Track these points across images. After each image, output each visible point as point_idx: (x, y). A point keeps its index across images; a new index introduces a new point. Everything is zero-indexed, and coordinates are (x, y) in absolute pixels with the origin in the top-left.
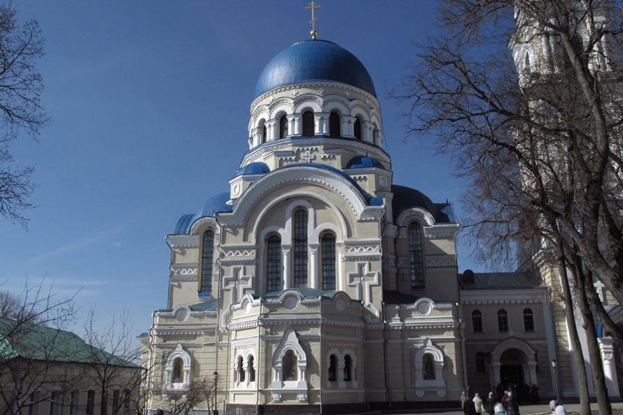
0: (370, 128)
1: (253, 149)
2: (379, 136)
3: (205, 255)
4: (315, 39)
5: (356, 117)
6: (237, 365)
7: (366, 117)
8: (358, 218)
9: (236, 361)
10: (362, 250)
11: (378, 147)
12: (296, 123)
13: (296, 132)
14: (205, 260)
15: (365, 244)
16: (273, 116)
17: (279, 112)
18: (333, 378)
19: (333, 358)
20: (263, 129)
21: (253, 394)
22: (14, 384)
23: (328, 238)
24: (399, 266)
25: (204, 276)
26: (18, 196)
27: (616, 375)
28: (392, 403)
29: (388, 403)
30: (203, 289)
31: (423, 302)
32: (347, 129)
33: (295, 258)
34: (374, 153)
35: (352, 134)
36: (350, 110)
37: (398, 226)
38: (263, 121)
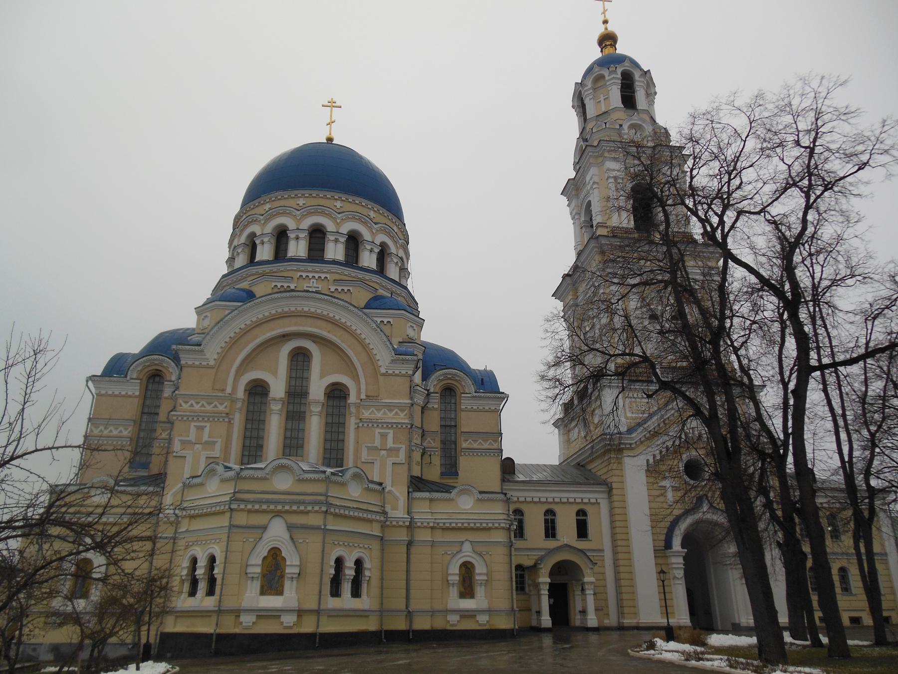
3: (146, 410)
9: (186, 563)
10: (397, 414)
14: (145, 417)
15: (390, 407)
21: (210, 616)
22: (626, 429)
23: (337, 393)
25: (141, 441)
27: (716, 602)
28: (413, 631)
29: (408, 631)
32: (368, 259)
33: (287, 420)
38: (253, 235)
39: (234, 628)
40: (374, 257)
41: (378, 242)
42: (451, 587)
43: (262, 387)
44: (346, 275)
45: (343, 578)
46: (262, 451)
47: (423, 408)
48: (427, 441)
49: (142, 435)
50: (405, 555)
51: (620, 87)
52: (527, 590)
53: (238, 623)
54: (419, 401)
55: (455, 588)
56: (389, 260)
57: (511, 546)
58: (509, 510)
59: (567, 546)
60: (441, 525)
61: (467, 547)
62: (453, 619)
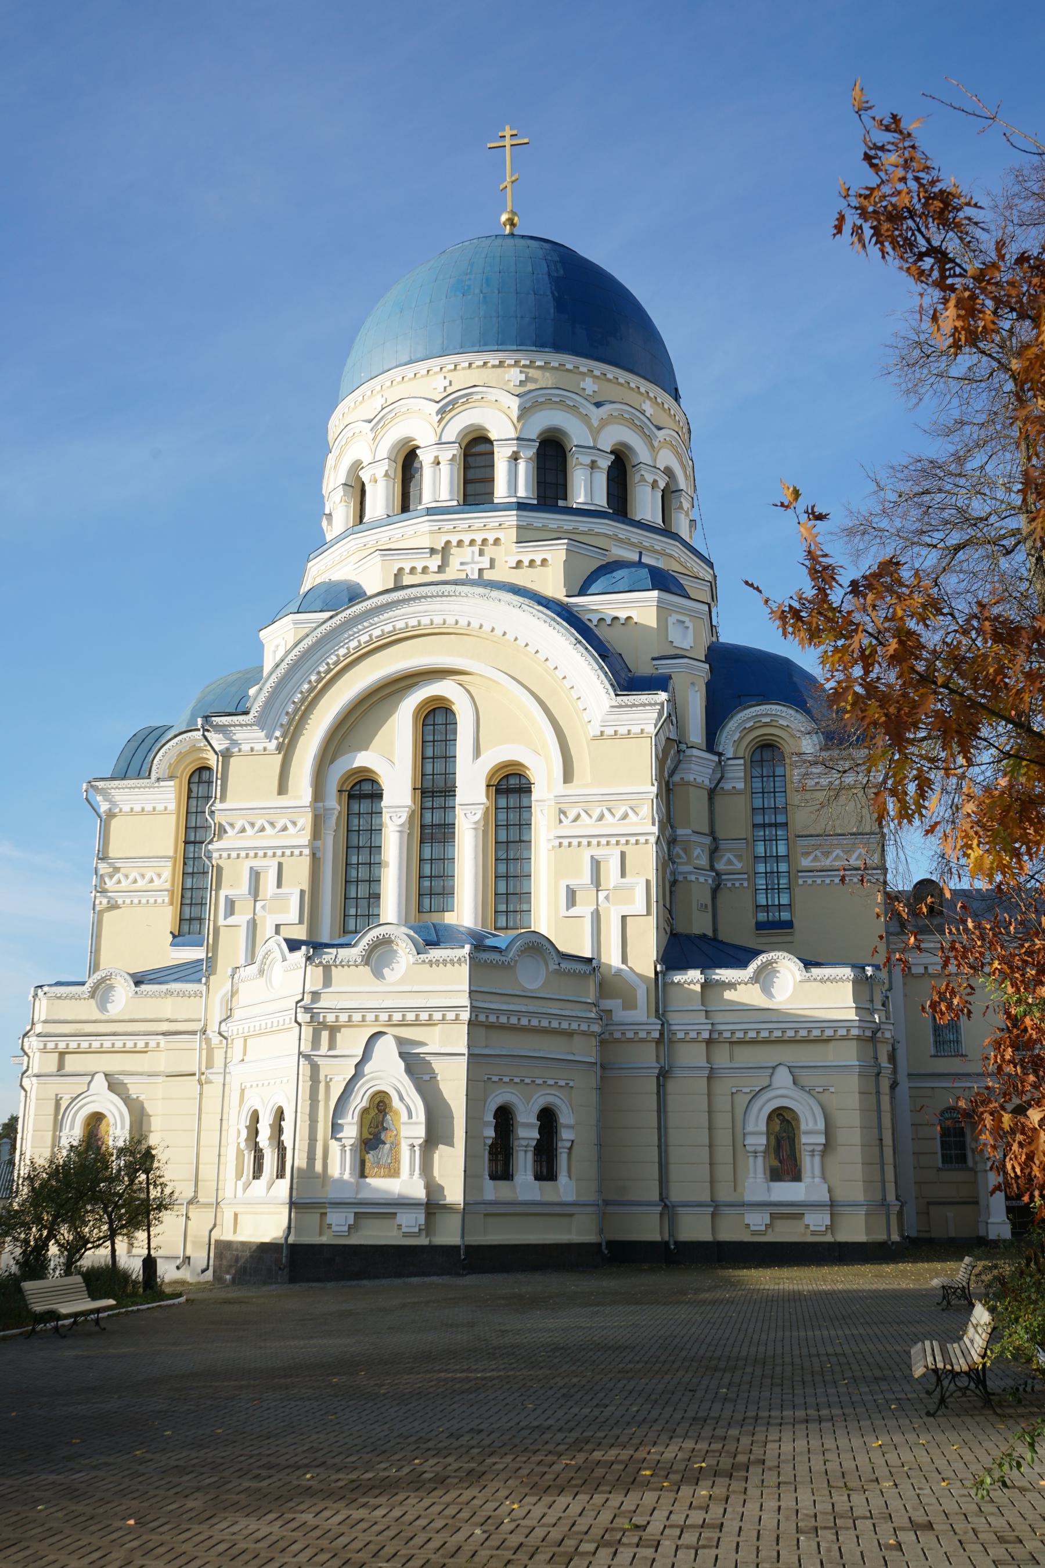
0: (593, 465)
1: (339, 539)
2: (681, 507)
4: (512, 235)
5: (612, 452)
6: (244, 1133)
7: (642, 452)
8: (594, 730)
9: (244, 1121)
11: (676, 537)
12: (522, 465)
13: (522, 492)
14: (191, 848)
16: (384, 450)
17: (393, 447)
18: (502, 1170)
19: (504, 1116)
20: (359, 491)
24: (720, 866)
25: (188, 894)
26: (999, 761)
28: (676, 1243)
30: (186, 928)
31: (769, 963)
34: (662, 554)
35: (601, 500)
36: (596, 433)
37: (720, 755)
39: (321, 1234)
40: (601, 480)
41: (607, 443)
42: (751, 1159)
44: (537, 529)
45: (516, 1143)
46: (379, 906)
47: (712, 793)
48: (725, 859)
49: (429, 769)
50: (655, 1097)
52: (970, 1163)
53: (324, 1227)
54: (699, 780)
55: (760, 1160)
56: (637, 478)
57: (878, 1074)
58: (872, 1001)
59: (356, 1066)
60: (727, 1035)
61: (783, 1077)
62: (757, 1220)
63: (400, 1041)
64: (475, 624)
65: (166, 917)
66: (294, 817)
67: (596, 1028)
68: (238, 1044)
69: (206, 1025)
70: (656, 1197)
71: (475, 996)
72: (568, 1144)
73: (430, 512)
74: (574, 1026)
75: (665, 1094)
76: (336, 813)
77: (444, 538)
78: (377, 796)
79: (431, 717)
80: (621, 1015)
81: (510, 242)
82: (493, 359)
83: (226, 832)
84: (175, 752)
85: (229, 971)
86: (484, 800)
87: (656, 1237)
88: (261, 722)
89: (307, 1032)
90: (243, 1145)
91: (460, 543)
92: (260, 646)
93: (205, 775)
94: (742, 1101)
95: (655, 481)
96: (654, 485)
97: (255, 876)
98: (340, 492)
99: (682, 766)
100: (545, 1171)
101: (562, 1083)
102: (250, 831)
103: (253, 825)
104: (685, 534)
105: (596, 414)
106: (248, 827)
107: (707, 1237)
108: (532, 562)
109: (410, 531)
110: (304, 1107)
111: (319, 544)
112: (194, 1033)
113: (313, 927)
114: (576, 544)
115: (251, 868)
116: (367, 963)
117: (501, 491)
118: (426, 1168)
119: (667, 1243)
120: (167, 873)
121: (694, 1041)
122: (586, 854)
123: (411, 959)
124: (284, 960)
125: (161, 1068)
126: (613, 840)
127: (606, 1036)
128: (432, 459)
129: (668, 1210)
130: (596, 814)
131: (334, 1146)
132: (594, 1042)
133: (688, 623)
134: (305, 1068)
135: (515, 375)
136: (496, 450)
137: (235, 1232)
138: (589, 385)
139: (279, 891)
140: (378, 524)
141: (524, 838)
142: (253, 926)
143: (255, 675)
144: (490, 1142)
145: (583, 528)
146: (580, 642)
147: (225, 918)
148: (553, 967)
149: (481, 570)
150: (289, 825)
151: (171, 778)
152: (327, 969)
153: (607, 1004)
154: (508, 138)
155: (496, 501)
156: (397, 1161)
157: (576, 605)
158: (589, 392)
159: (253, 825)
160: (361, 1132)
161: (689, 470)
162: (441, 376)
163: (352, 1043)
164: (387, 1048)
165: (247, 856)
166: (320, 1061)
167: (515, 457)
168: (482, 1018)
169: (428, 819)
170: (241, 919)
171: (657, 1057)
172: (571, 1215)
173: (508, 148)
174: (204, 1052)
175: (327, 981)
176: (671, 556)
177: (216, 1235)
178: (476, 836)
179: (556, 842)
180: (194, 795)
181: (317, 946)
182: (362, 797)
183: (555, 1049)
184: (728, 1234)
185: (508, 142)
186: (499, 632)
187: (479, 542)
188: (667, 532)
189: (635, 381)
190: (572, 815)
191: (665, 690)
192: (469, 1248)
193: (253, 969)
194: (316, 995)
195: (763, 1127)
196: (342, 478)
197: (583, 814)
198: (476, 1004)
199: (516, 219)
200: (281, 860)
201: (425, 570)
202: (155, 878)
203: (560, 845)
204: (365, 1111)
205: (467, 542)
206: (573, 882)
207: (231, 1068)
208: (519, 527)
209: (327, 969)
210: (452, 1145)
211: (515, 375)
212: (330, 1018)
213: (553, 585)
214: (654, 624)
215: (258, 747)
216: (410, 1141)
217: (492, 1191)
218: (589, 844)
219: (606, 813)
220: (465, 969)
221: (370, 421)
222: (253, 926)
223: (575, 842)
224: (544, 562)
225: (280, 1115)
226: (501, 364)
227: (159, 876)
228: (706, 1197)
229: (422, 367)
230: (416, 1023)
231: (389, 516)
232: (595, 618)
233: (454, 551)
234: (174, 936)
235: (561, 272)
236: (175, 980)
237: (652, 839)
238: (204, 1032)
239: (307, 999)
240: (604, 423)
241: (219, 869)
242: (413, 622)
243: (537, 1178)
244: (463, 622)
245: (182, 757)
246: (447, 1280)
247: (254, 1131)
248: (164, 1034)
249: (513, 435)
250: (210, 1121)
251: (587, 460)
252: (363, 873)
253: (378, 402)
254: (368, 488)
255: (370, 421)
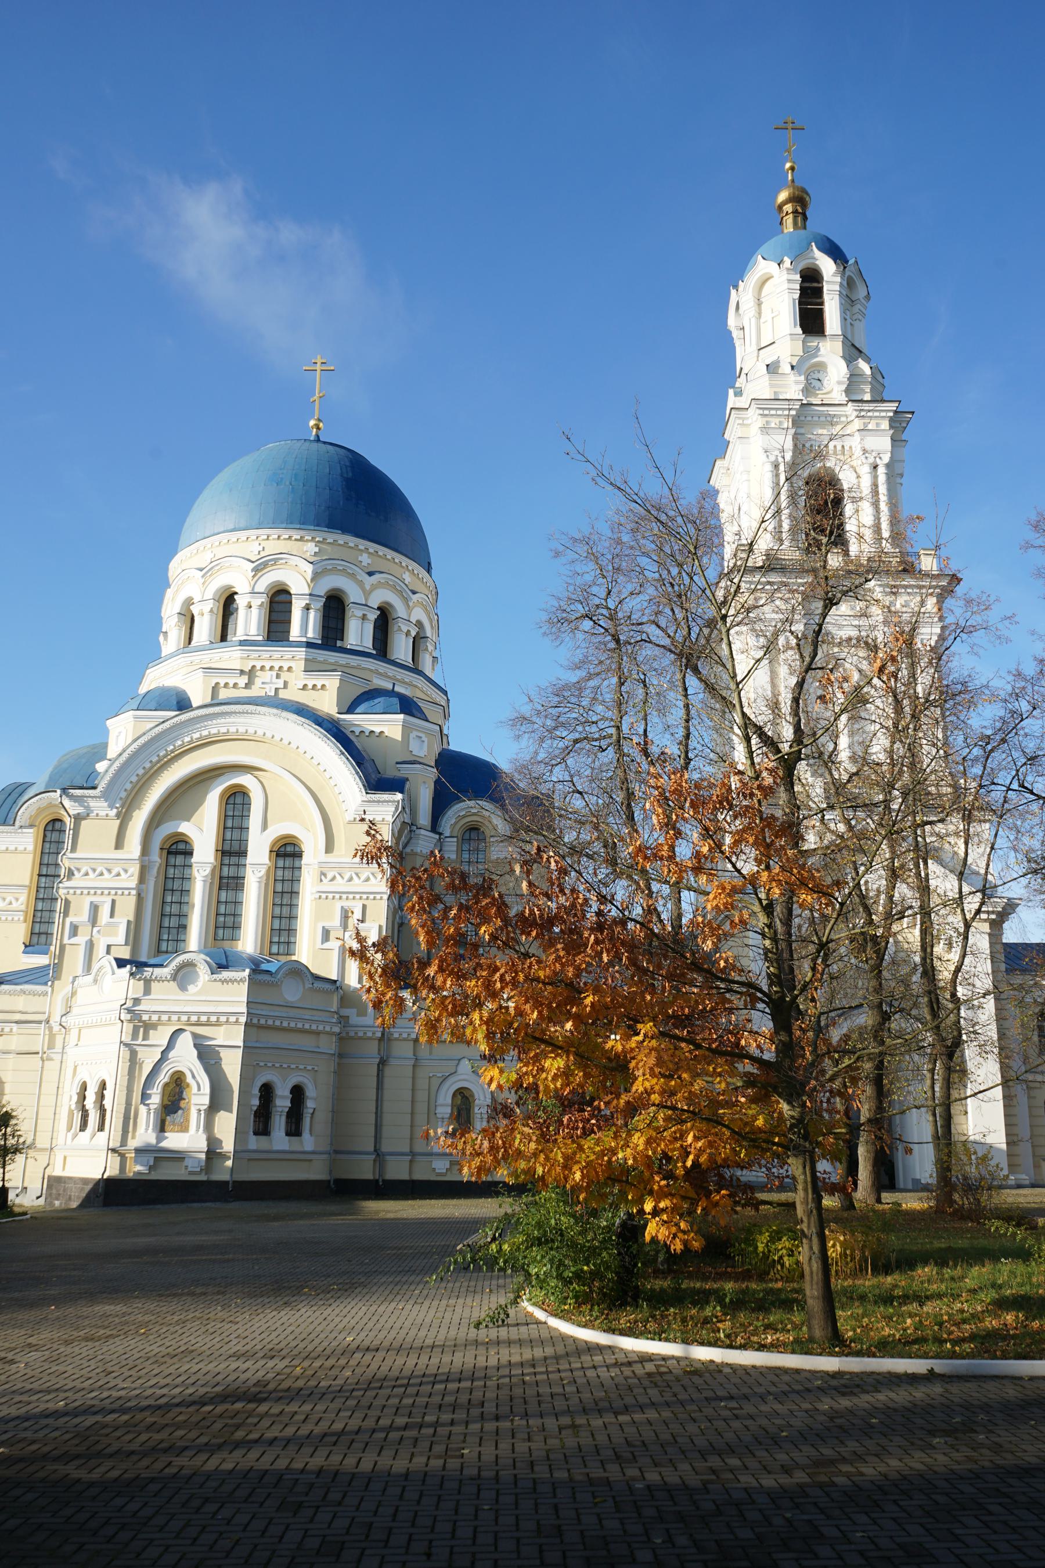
0: (408, 633)
1: (172, 656)
2: (427, 649)
6: (75, 1098)
7: (400, 609)
9: (76, 1089)
11: (420, 673)
12: (312, 614)
14: (43, 879)
16: (210, 593)
19: (267, 1092)
25: (39, 914)
28: (384, 1181)
32: (401, 648)
34: (410, 684)
35: (368, 644)
36: (367, 594)
37: (440, 834)
40: (369, 628)
41: (375, 601)
43: (186, 842)
44: (320, 662)
45: (274, 1109)
46: (185, 934)
49: (228, 836)
50: (375, 1079)
51: (797, 296)
56: (396, 628)
59: (162, 1052)
63: (195, 1036)
64: (269, 735)
65: (20, 932)
66: (126, 866)
67: (337, 1029)
68: (74, 1033)
69: (49, 1017)
70: (372, 1149)
71: (252, 1005)
72: (311, 1111)
73: (242, 643)
74: (321, 1028)
75: (383, 1077)
76: (158, 865)
77: (251, 663)
78: (189, 853)
79: (232, 798)
80: (355, 1020)
81: (315, 445)
82: (296, 535)
83: (73, 874)
84: (36, 807)
85: (71, 979)
86: (267, 861)
87: (370, 1177)
88: (105, 795)
89: (128, 1028)
90: (73, 1107)
91: (262, 668)
92: (106, 732)
93: (58, 825)
94: (435, 1083)
95: (409, 631)
96: (408, 633)
97: (95, 909)
98: (175, 619)
99: (412, 841)
100: (293, 1128)
101: (309, 1068)
102: (92, 875)
103: (94, 870)
104: (428, 672)
105: (369, 581)
106: (90, 872)
107: (405, 1177)
108: (314, 686)
109: (226, 655)
110: (123, 1081)
111: (155, 656)
112: (40, 1022)
113: (134, 950)
114: (347, 675)
115: (91, 903)
116: (174, 980)
117: (295, 632)
118: (209, 1126)
119: (377, 1181)
120: (23, 898)
121: (405, 1040)
122: (338, 905)
123: (207, 978)
124: (113, 973)
125: (13, 1047)
126: (358, 896)
127: (344, 1035)
128: (246, 604)
129: (379, 1155)
130: (347, 877)
131: (143, 1109)
132: (334, 1039)
133: (424, 738)
134: (126, 1053)
135: (311, 548)
136: (294, 601)
137: (64, 1169)
138: (365, 559)
139: (112, 920)
140: (201, 649)
141: (295, 890)
142: (91, 945)
143: (99, 752)
144: (255, 1108)
145: (353, 663)
146: (343, 754)
147: (69, 938)
148: (308, 985)
149: (277, 689)
150: (122, 873)
151: (31, 826)
152: (148, 982)
153: (345, 1012)
154: (318, 365)
155: (291, 639)
156: (188, 1120)
157: (344, 720)
158: (364, 564)
159: (94, 870)
160: (162, 1100)
161: (435, 623)
162: (257, 543)
163: (160, 1037)
164: (185, 1042)
165: (89, 893)
166: (138, 1049)
167: (307, 608)
168: (255, 1021)
169: (225, 873)
170: (81, 939)
171: (379, 1050)
172: (310, 1161)
173: (318, 372)
174: (47, 1037)
175: (147, 991)
176: (416, 686)
177: (48, 1172)
178: (260, 888)
179: (317, 895)
180: (48, 839)
181: (141, 965)
182: (177, 853)
183: (306, 1042)
184: (419, 1175)
185: (318, 367)
186: (285, 742)
187: (277, 668)
188: (417, 671)
189: (398, 558)
190: (330, 876)
191: (402, 792)
192: (234, 1182)
193: (90, 978)
194: (137, 1001)
195: (449, 1101)
196: (177, 608)
197: (338, 876)
198: (251, 1011)
199: (321, 425)
200: (115, 897)
201: (235, 685)
202: (14, 901)
203: (320, 897)
204: (166, 1085)
205: (268, 668)
206: (327, 924)
207: (67, 1049)
208: (306, 660)
209: (148, 982)
210: (231, 1112)
211: (311, 548)
212: (145, 1017)
213: (327, 703)
214: (399, 738)
215: (102, 813)
216: (198, 1107)
217: (254, 1142)
218: (340, 898)
219: (354, 876)
220: (245, 987)
221: (201, 570)
222: (91, 945)
223: (330, 896)
224: (323, 686)
225: (103, 1086)
226: (301, 539)
227: (17, 899)
228: (408, 1150)
229: (243, 535)
230: (208, 1024)
231: (212, 643)
232: (357, 731)
233: (258, 673)
234: (26, 946)
235: (350, 474)
236: (26, 982)
237: (386, 897)
238: (48, 1022)
239: (129, 1004)
240: (374, 587)
241: (67, 903)
242: (223, 730)
243: (287, 1134)
244: (260, 733)
245: (40, 811)
246: (218, 1205)
247: (82, 1097)
248: (16, 1022)
249: (307, 591)
250: (49, 1087)
251: (360, 614)
252: (175, 909)
253: (208, 556)
254: (196, 619)
255: (201, 570)
